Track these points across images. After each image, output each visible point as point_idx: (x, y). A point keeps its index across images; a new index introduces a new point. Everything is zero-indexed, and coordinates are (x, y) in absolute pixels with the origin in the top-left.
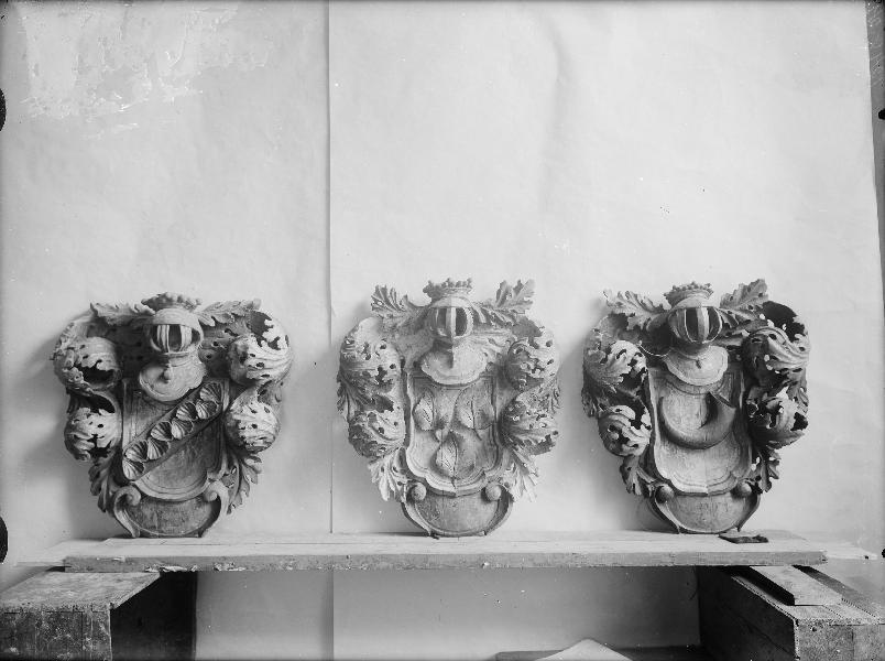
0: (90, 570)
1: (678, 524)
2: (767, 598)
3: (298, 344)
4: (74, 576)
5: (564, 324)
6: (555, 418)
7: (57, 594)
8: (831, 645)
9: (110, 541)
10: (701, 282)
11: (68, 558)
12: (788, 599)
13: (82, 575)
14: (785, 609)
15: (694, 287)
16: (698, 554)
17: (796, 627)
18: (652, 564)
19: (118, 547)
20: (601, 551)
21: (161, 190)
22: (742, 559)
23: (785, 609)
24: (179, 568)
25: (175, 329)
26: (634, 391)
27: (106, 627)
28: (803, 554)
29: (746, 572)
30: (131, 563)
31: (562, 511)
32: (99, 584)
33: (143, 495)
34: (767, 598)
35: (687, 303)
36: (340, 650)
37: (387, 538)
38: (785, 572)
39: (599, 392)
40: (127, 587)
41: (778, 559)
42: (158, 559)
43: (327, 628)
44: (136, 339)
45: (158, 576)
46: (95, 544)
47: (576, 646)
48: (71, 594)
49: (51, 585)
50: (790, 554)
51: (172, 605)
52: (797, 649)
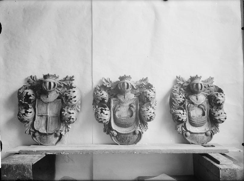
0: (26, 154)
2: (212, 162)
7: (17, 160)
12: (218, 162)
13: (24, 155)
14: (216, 164)
17: (220, 170)
23: (216, 164)
28: (223, 150)
29: (207, 155)
30: (38, 152)
34: (212, 162)
38: (217, 155)
40: (37, 158)
41: (215, 152)
42: (45, 151)
45: (45, 155)
48: (20, 160)
49: (15, 158)
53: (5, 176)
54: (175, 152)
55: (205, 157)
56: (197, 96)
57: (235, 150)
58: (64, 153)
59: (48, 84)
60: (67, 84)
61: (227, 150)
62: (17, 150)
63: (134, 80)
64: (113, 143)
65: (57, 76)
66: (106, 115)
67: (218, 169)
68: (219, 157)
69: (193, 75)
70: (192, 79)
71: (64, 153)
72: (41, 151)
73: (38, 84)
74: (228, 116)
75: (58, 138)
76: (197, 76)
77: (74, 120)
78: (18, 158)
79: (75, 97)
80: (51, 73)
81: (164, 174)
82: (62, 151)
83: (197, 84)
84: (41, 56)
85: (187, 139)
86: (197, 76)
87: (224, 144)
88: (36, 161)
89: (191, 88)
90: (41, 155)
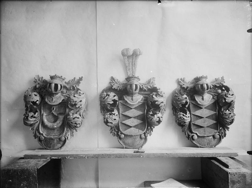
0: (31, 158)
1: (198, 145)
2: (222, 167)
3: (92, 89)
4: (27, 160)
5: (167, 88)
6: (165, 115)
7: (22, 165)
8: (239, 179)
9: (36, 150)
10: (205, 76)
11: (25, 155)
12: (227, 166)
13: (29, 160)
14: (225, 168)
15: (202, 77)
16: (201, 154)
17: (229, 174)
18: (192, 156)
19: (38, 151)
20: (174, 153)
21: (56, 48)
22: (214, 155)
23: (225, 168)
24: (56, 158)
25: (56, 85)
26: (184, 109)
27: (36, 174)
28: (232, 154)
29: (215, 159)
30: (43, 156)
31: (164, 140)
32: (34, 162)
33: (198, 136)
34: (222, 167)
35: (201, 82)
36: (100, 184)
37: (114, 149)
38: (226, 159)
39: (178, 108)
40: (41, 163)
41: (224, 155)
42: (50, 155)
43: (97, 180)
44: (44, 88)
45: (50, 160)
46: (32, 151)
47: (167, 180)
48: (26, 165)
49: (20, 163)
50: (227, 154)
51: (54, 170)
52: (229, 181)
53: (10, 181)
54: (182, 156)
55: (213, 161)
56: (203, 96)
57: (243, 154)
58: (69, 157)
59: (53, 85)
60: (73, 87)
61: (236, 153)
62: (22, 155)
63: (209, 81)
64: (121, 146)
65: (63, 77)
66: (115, 118)
67: (227, 173)
68: (228, 161)
69: (199, 75)
70: (197, 80)
71: (69, 157)
72: (46, 155)
73: (43, 85)
74: (236, 118)
75: (62, 143)
76: (61, 77)
77: (80, 125)
78: (23, 163)
79: (81, 101)
80: (59, 74)
81: (170, 180)
82: (26, 90)
83: (202, 85)
84: (44, 57)
85: (194, 142)
86: (61, 77)
87: (230, 146)
88: (41, 166)
89: (196, 90)
90: (46, 159)
